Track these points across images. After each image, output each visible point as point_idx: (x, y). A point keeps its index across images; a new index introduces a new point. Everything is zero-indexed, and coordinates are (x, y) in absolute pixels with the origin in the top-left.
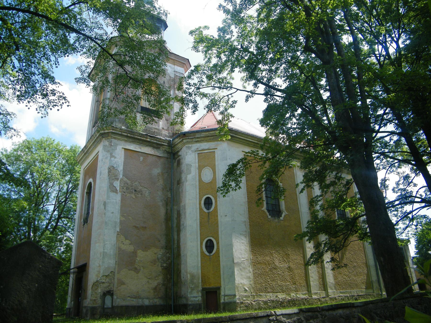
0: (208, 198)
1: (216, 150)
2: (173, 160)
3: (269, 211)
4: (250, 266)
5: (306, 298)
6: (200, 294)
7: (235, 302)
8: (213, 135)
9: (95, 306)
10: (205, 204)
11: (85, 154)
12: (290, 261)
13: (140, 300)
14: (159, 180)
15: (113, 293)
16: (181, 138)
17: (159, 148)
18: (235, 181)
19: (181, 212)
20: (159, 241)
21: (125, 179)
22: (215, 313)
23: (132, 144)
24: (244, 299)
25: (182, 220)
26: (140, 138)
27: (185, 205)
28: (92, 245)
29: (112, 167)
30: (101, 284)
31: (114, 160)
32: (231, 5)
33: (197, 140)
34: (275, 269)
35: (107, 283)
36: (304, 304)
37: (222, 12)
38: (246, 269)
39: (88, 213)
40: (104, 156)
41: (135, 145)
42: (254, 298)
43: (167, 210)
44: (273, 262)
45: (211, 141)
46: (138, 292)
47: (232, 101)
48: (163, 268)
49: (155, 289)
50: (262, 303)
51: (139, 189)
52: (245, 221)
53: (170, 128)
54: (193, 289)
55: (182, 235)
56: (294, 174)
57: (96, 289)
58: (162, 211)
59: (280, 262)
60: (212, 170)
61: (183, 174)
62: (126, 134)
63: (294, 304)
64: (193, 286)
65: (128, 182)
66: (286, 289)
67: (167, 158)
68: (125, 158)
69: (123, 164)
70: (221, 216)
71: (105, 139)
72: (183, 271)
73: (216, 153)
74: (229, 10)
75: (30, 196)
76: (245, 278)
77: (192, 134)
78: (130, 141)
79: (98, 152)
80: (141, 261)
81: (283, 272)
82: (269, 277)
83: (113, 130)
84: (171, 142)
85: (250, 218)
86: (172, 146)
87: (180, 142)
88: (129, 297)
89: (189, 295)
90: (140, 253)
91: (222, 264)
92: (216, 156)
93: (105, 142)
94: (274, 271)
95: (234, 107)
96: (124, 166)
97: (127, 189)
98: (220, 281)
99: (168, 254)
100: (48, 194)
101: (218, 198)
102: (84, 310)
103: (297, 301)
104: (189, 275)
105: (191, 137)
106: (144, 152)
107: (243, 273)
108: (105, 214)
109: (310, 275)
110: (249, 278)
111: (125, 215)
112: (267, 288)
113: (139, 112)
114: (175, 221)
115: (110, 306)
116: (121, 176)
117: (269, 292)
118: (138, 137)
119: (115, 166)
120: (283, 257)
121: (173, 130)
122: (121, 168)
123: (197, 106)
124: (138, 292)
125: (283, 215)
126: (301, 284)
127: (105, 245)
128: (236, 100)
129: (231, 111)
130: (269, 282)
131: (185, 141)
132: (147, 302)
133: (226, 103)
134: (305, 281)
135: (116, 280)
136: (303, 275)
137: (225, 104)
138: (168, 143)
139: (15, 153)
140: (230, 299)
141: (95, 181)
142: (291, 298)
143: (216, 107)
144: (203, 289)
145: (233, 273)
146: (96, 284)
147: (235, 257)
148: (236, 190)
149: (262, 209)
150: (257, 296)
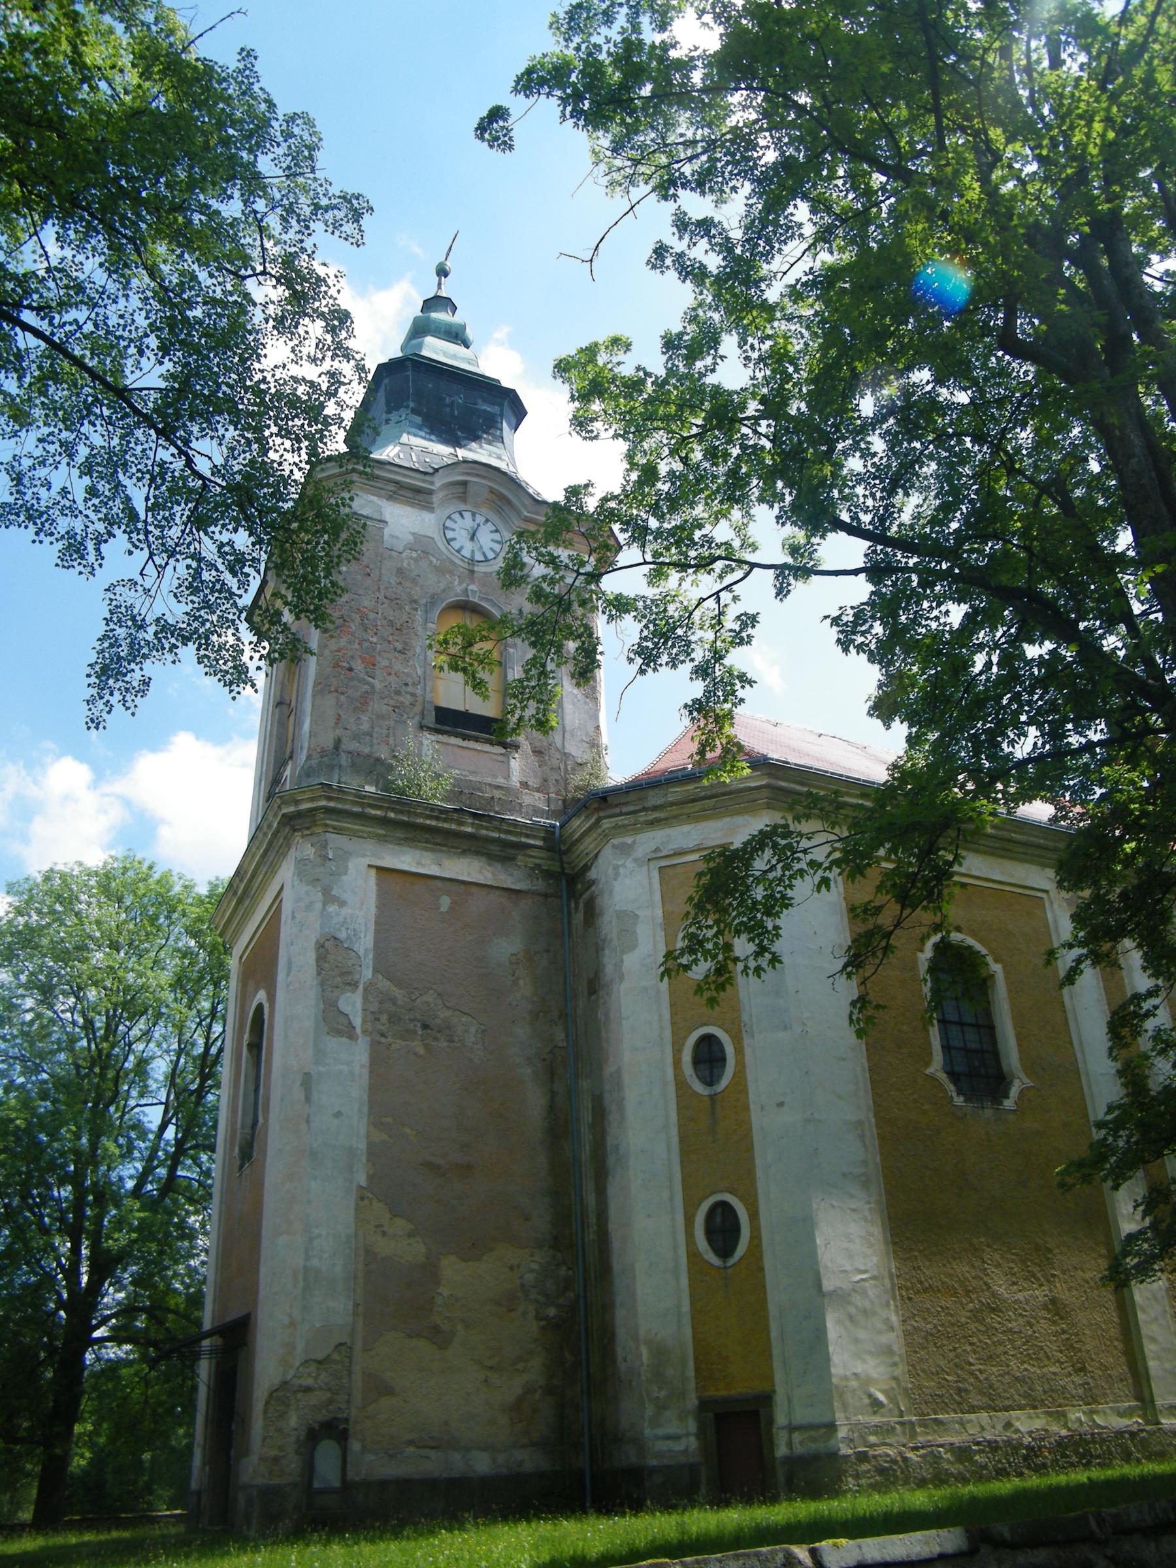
0: (708, 1041)
2: (569, 900)
3: (953, 1076)
4: (888, 1305)
5: (1135, 1428)
6: (692, 1425)
7: (833, 1455)
8: (714, 791)
9: (276, 1481)
10: (697, 1061)
11: (240, 902)
12: (1054, 1276)
13: (457, 1456)
14: (515, 983)
15: (346, 1431)
17: (512, 859)
18: (750, 930)
19: (607, 1101)
20: (527, 1219)
21: (384, 984)
22: (748, 1500)
24: (872, 1439)
25: (613, 1131)
26: (434, 823)
27: (619, 1071)
28: (265, 1243)
29: (332, 942)
30: (300, 1396)
31: (338, 915)
32: (708, 247)
33: (653, 816)
34: (993, 1310)
35: (321, 1388)
36: (1127, 1457)
37: (672, 275)
38: (874, 1314)
39: (255, 1123)
40: (299, 900)
41: (417, 853)
42: (913, 1435)
43: (553, 1094)
44: (986, 1284)
46: (446, 1423)
47: (738, 618)
48: (543, 1323)
49: (516, 1407)
50: (948, 1456)
51: (438, 1021)
52: (859, 1124)
53: (552, 783)
54: (661, 1407)
55: (612, 1190)
56: (1047, 925)
57: (282, 1416)
58: (535, 1101)
59: (1014, 1283)
62: (378, 813)
63: (1083, 1456)
65: (398, 993)
66: (1045, 1392)
67: (546, 896)
68: (382, 905)
69: (372, 926)
70: (762, 1108)
71: (303, 837)
72: (621, 1333)
74: (703, 267)
75: (78, 1073)
76: (870, 1353)
77: (632, 797)
78: (399, 839)
80: (457, 1300)
81: (1029, 1323)
82: (972, 1344)
83: (330, 799)
85: (879, 1109)
86: (563, 848)
87: (590, 829)
88: (411, 1442)
89: (648, 1432)
90: (452, 1269)
93: (304, 848)
94: (993, 1320)
95: (749, 643)
96: (377, 932)
97: (394, 1019)
98: (771, 1369)
99: (564, 1268)
100: (142, 1064)
102: (241, 1501)
103: (1094, 1442)
104: (644, 1351)
105: (631, 808)
106: (454, 876)
107: (862, 1334)
108: (308, 1121)
109: (1145, 1330)
110: (889, 1351)
111: (389, 1120)
112: (966, 1390)
113: (429, 729)
114: (587, 1137)
115: (336, 1483)
116: (367, 974)
117: (973, 1409)
119: (343, 935)
120: (1023, 1262)
121: (566, 789)
122: (365, 943)
123: (595, 650)
124: (446, 1423)
125: (1014, 1092)
126: (1107, 1368)
127: (311, 1240)
128: (751, 612)
129: (736, 659)
130: (971, 1364)
131: (606, 824)
132: (483, 1464)
133: (712, 626)
134: (1123, 1359)
135: (357, 1376)
136: (1114, 1332)
137: (710, 635)
138: (544, 839)
139: (21, 920)
140: (814, 1440)
141: (272, 998)
142: (1069, 1429)
143: (674, 651)
145: (820, 1334)
146: (282, 1394)
147: (826, 1267)
148: (758, 970)
149: (927, 1072)
150: (925, 1426)
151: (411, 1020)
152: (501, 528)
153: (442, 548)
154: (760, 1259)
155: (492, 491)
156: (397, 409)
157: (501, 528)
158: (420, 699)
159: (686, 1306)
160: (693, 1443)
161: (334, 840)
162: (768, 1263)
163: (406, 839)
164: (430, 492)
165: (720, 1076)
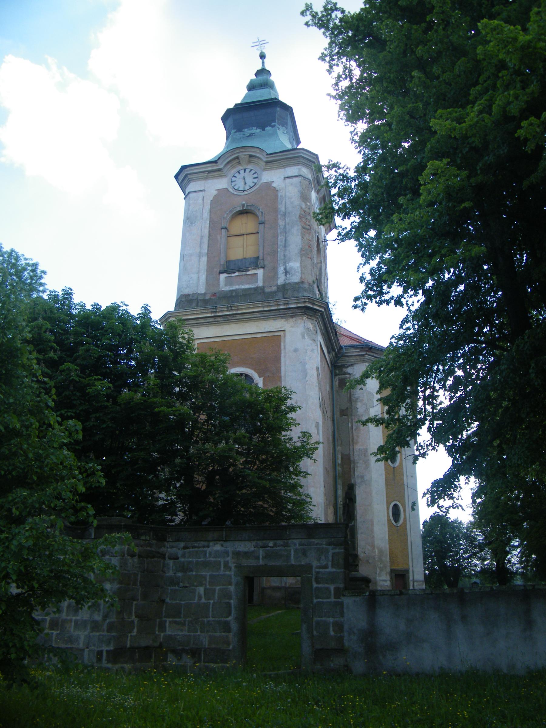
6: (388, 578)
16: (364, 351)
54: (381, 570)
71: (307, 318)
77: (379, 352)
89: (378, 578)
104: (377, 551)
105: (376, 356)
131: (367, 357)
144: (392, 571)
154: (406, 525)
160: (388, 583)
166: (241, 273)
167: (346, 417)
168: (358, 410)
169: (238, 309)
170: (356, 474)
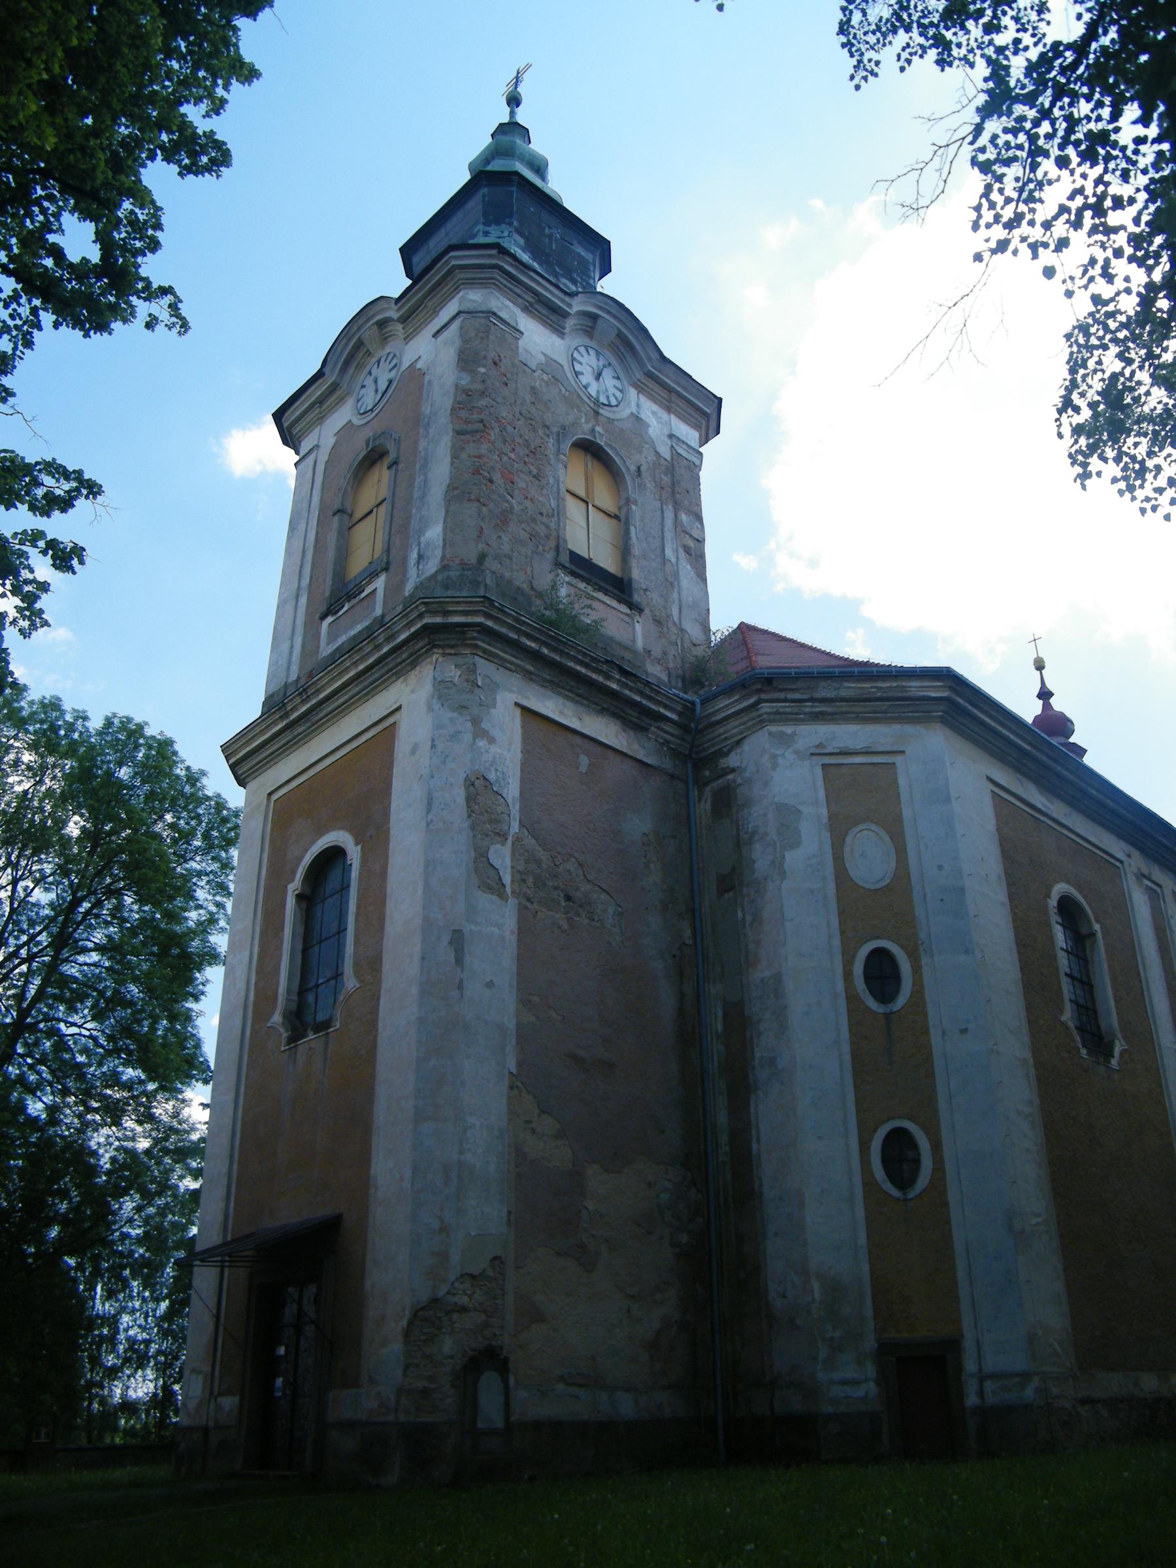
0: (880, 955)
1: (898, 760)
6: (870, 1370)
8: (891, 694)
10: (868, 977)
16: (750, 695)
21: (530, 841)
23: (549, 693)
27: (778, 978)
30: (455, 1316)
45: (875, 721)
48: (677, 1250)
60: (887, 839)
61: (758, 847)
64: (837, 1334)
65: (541, 854)
67: (672, 777)
70: (944, 1033)
71: (444, 655)
73: (899, 771)
77: (800, 684)
78: (544, 680)
79: (399, 708)
83: (488, 616)
84: (698, 707)
85: (1035, 1051)
88: (561, 1378)
89: (821, 1376)
91: (959, 1236)
92: (902, 781)
101: (922, 953)
104: (816, 1285)
105: (796, 696)
108: (460, 986)
113: (564, 567)
115: (500, 1424)
116: (515, 827)
118: (578, 668)
119: (492, 776)
122: (512, 790)
125: (1117, 1052)
131: (766, 708)
138: (680, 714)
144: (884, 1349)
151: (556, 888)
152: (622, 376)
153: (571, 378)
154: (944, 1193)
155: (620, 335)
156: (498, 223)
157: (622, 376)
158: (554, 534)
159: (862, 1240)
160: (871, 1388)
161: (485, 667)
162: (953, 1197)
163: (552, 682)
164: (564, 315)
165: (897, 991)
166: (354, 601)
167: (731, 894)
168: (756, 866)
169: (318, 691)
170: (758, 1055)
